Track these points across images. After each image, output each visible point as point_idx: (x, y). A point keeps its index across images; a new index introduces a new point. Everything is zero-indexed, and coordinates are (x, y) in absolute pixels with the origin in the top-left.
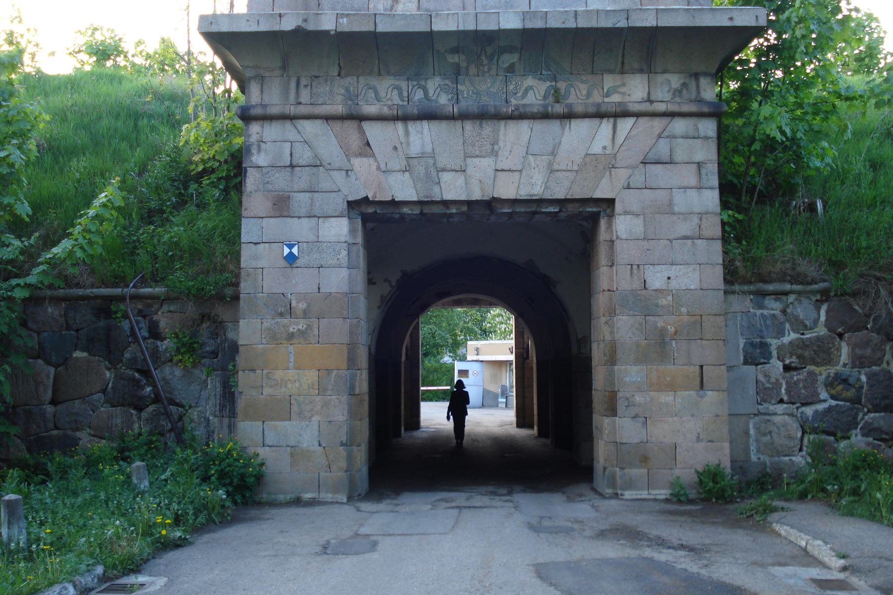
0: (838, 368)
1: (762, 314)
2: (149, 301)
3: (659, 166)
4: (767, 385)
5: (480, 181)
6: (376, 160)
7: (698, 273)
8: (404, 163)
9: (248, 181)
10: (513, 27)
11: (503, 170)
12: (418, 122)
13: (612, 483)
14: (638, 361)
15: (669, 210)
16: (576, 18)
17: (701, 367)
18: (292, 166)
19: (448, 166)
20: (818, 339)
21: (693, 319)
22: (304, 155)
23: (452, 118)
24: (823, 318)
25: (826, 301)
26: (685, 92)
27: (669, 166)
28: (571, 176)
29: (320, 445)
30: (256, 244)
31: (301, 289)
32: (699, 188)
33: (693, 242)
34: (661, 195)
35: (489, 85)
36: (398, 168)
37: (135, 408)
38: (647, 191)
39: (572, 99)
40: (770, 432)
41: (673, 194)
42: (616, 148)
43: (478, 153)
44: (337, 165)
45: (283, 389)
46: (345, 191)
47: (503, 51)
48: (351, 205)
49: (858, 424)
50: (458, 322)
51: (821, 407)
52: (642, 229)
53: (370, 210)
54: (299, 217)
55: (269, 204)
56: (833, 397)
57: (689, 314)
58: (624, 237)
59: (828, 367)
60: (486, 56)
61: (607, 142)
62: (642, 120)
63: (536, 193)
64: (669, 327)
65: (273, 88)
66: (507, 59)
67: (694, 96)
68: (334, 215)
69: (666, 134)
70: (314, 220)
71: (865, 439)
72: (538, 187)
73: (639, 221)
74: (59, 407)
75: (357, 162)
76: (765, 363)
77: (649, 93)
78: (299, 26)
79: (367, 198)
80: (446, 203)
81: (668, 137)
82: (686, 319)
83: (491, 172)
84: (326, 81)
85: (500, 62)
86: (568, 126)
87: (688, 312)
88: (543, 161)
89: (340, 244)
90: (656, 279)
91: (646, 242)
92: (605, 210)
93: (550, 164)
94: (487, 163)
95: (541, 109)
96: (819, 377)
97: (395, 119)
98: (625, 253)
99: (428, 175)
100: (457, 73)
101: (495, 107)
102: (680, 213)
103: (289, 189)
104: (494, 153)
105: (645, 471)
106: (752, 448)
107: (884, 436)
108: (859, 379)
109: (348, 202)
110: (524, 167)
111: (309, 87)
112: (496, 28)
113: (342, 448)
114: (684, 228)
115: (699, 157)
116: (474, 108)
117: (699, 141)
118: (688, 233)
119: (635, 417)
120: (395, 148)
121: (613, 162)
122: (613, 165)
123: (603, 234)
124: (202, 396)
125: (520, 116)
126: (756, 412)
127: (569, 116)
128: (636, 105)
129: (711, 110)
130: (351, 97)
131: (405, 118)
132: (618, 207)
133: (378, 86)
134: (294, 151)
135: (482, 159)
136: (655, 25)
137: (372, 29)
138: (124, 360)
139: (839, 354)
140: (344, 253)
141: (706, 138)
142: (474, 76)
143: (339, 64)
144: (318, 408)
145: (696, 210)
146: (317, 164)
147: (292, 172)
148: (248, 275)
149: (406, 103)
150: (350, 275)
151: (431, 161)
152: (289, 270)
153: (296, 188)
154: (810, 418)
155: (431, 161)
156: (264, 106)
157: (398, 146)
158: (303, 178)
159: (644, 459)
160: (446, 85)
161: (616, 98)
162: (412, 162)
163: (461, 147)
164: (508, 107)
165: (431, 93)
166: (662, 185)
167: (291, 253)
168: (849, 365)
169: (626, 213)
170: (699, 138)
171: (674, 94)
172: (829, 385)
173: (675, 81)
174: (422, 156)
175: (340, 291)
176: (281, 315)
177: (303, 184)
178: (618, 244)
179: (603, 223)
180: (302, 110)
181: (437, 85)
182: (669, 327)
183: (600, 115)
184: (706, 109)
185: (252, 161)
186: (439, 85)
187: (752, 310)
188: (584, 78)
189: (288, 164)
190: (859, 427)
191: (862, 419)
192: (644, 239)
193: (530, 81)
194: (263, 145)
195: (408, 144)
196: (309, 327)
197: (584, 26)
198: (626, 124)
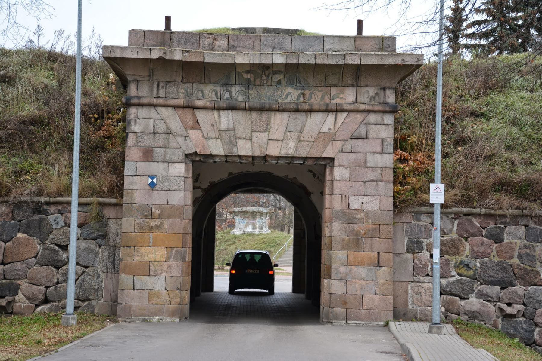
0: (462, 257)
1: (418, 224)
2: (65, 205)
3: (360, 140)
4: (420, 265)
5: (260, 145)
6: (202, 131)
7: (378, 201)
8: (217, 134)
9: (129, 140)
10: (280, 62)
11: (272, 140)
12: (226, 111)
13: (328, 318)
14: (343, 249)
15: (364, 165)
16: (315, 58)
17: (379, 253)
18: (154, 133)
19: (242, 137)
20: (451, 240)
21: (375, 226)
23: (245, 109)
24: (455, 228)
25: (457, 218)
26: (377, 98)
27: (365, 140)
28: (310, 144)
29: (165, 289)
30: (133, 176)
31: (157, 202)
32: (382, 153)
33: (377, 184)
34: (361, 157)
35: (266, 91)
36: (214, 136)
37: (55, 267)
38: (352, 154)
39: (313, 100)
40: (420, 292)
41: (367, 156)
42: (336, 129)
43: (259, 130)
44: (180, 133)
45: (146, 258)
46: (184, 148)
47: (275, 73)
49: (474, 291)
50: (103, 129)
51: (451, 279)
52: (349, 176)
53: (198, 159)
54: (158, 162)
55: (141, 154)
56: (459, 274)
57: (372, 223)
58: (338, 179)
59: (457, 257)
60: (265, 75)
61: (332, 127)
62: (351, 114)
63: (290, 153)
64: (361, 230)
65: (144, 88)
66: (277, 77)
67: (382, 100)
68: (178, 161)
69: (365, 122)
70: (166, 164)
71: (478, 300)
72: (292, 150)
73: (347, 171)
74: (6, 266)
75: (191, 132)
76: (419, 252)
77: (356, 99)
78: (161, 57)
79: (196, 152)
80: (240, 157)
81: (365, 124)
82: (371, 226)
83: (265, 140)
84: (174, 85)
85: (273, 79)
86: (309, 116)
87: (372, 222)
88: (295, 135)
89: (180, 178)
90: (355, 203)
91: (350, 183)
92: (329, 163)
93: (299, 137)
94: (264, 135)
95: (295, 107)
96: (451, 262)
97: (214, 109)
98: (338, 187)
99: (231, 141)
100: (248, 84)
101: (269, 104)
102: (370, 167)
103: (152, 146)
104: (268, 130)
105: (344, 310)
106: (409, 301)
107: (490, 299)
108: (475, 265)
109: (186, 155)
110: (284, 138)
111: (165, 88)
112: (271, 62)
113: (177, 291)
114: (373, 175)
115: (383, 135)
116: (257, 105)
117: (383, 126)
118: (375, 178)
119: (341, 279)
120: (213, 125)
121: (334, 138)
122: (334, 139)
123: (328, 177)
124: (96, 261)
125: (282, 110)
126: (413, 281)
127: (311, 111)
128: (348, 105)
129: (391, 109)
130: (189, 95)
131: (219, 109)
132: (336, 162)
133: (204, 90)
134: (155, 125)
135: (261, 133)
136: (359, 63)
137: (202, 60)
138: (49, 239)
139: (464, 249)
140: (182, 183)
141: (388, 125)
142: (258, 85)
143: (182, 76)
144: (165, 269)
145: (380, 165)
146: (168, 132)
147: (154, 136)
148: (128, 193)
149: (219, 100)
150: (185, 195)
151: (232, 133)
152: (151, 191)
153: (156, 145)
154: (445, 286)
155: (232, 133)
156: (139, 98)
157: (215, 124)
158: (161, 140)
159: (345, 303)
160: (242, 90)
161: (337, 101)
162: (221, 133)
163: (249, 126)
164: (276, 105)
165: (234, 94)
166: (361, 151)
167: (152, 182)
168: (470, 256)
169: (340, 166)
170: (383, 125)
171: (371, 99)
172: (457, 266)
173: (372, 91)
174: (228, 130)
175: (179, 204)
176: (146, 216)
177: (160, 144)
178: (335, 182)
179: (328, 170)
180: (161, 101)
181: (237, 89)
182: (361, 230)
183: (328, 111)
184: (388, 109)
185: (131, 129)
186: (239, 91)
187: (413, 222)
188: (320, 88)
189: (152, 131)
190: (475, 292)
191: (476, 288)
192: (349, 181)
193: (289, 90)
194: (138, 120)
195: (220, 123)
196: (162, 223)
197: (320, 63)
198: (342, 116)
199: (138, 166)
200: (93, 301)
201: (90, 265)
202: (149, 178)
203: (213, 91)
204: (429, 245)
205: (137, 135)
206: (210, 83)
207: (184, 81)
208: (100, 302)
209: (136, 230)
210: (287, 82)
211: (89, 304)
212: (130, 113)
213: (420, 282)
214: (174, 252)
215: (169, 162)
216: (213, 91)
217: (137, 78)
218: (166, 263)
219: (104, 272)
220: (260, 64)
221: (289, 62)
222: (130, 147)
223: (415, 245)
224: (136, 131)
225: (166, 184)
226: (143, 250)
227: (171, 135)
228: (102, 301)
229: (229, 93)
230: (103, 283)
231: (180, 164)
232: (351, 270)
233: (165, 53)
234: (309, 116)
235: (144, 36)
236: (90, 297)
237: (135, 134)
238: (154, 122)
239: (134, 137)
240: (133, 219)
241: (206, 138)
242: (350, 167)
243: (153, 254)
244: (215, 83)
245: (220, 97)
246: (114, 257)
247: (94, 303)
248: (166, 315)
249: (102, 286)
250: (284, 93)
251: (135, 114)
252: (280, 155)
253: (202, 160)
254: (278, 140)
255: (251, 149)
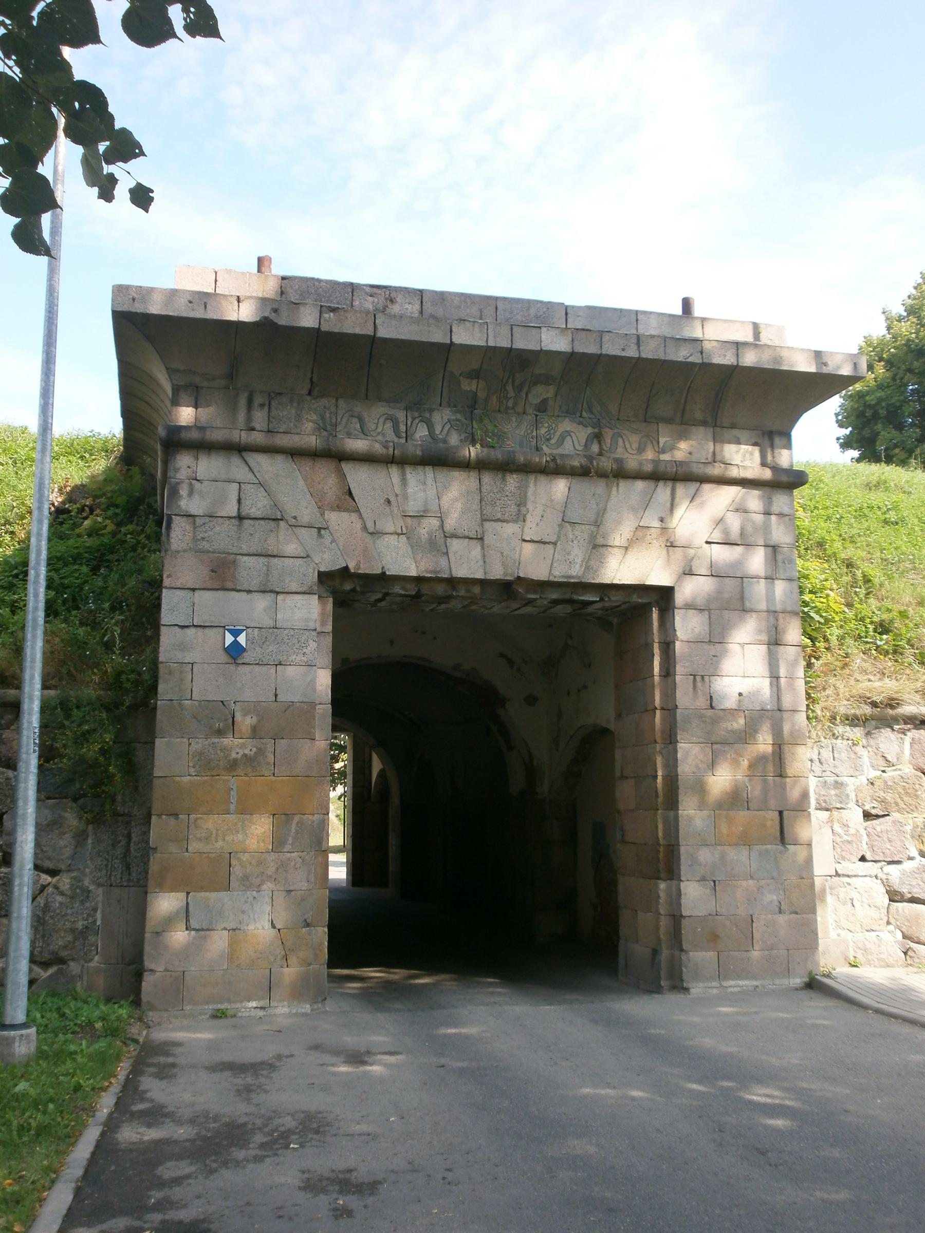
12: (420, 468)
17: (781, 813)
22: (257, 504)
31: (249, 695)
43: (499, 516)
45: (220, 843)
47: (537, 381)
48: (324, 577)
59: (915, 815)
60: (513, 385)
63: (575, 574)
70: (269, 597)
75: (334, 518)
78: (266, 318)
79: (346, 568)
84: (291, 401)
88: (583, 533)
93: (593, 537)
103: (235, 550)
110: (559, 537)
111: (266, 408)
125: (554, 470)
127: (621, 474)
132: (680, 597)
133: (365, 415)
134: (243, 496)
135: (505, 524)
143: (311, 380)
144: (271, 870)
147: (240, 525)
149: (403, 441)
152: (232, 667)
153: (245, 549)
157: (392, 499)
160: (457, 420)
164: (541, 456)
165: (438, 430)
167: (236, 643)
180: (258, 438)
181: (446, 418)
186: (449, 421)
192: (710, 641)
193: (566, 425)
194: (197, 485)
195: (406, 498)
196: (261, 751)
199: (196, 601)
200: (72, 964)
201: (63, 867)
202: (227, 634)
203: (387, 419)
204: (861, 791)
205: (194, 523)
206: (380, 399)
207: (315, 393)
208: (92, 964)
209: (192, 771)
210: (560, 407)
211: (60, 971)
212: (177, 466)
213: (848, 876)
214: (294, 826)
215: (278, 593)
216: (387, 419)
217: (197, 380)
218: (273, 856)
219: (99, 885)
220: (510, 350)
221: (580, 349)
222: (178, 552)
223: (833, 792)
224: (194, 511)
225: (273, 648)
226: (210, 823)
227: (282, 523)
228: (96, 961)
229: (425, 426)
230: (99, 915)
231: (307, 597)
232: (723, 857)
233: (275, 311)
234: (614, 489)
235: (216, 281)
236: (64, 954)
237: (191, 519)
238: (240, 489)
239: (189, 528)
240: (185, 740)
241: (371, 534)
242: (709, 610)
243: (238, 832)
244: (393, 400)
245: (404, 435)
246: (129, 843)
247: (74, 967)
248: (275, 994)
249: (95, 922)
250: (555, 432)
251: (190, 470)
252: (552, 579)
253: (358, 589)
254: (545, 543)
255: (481, 563)
